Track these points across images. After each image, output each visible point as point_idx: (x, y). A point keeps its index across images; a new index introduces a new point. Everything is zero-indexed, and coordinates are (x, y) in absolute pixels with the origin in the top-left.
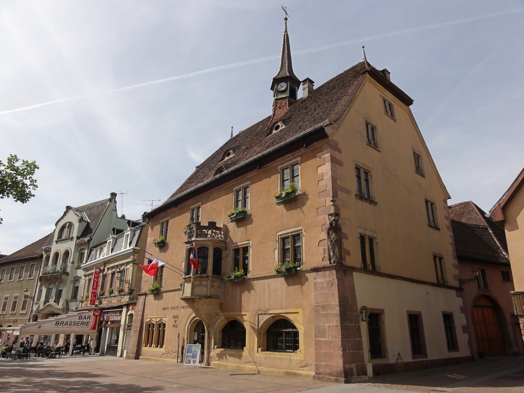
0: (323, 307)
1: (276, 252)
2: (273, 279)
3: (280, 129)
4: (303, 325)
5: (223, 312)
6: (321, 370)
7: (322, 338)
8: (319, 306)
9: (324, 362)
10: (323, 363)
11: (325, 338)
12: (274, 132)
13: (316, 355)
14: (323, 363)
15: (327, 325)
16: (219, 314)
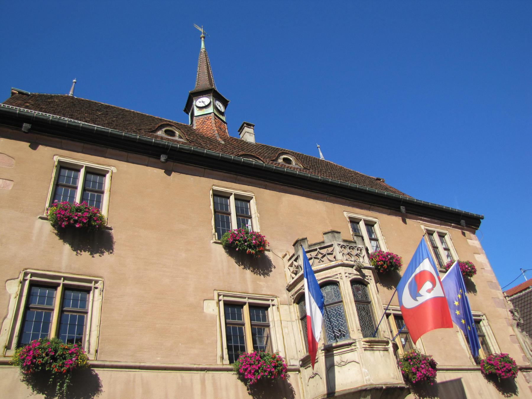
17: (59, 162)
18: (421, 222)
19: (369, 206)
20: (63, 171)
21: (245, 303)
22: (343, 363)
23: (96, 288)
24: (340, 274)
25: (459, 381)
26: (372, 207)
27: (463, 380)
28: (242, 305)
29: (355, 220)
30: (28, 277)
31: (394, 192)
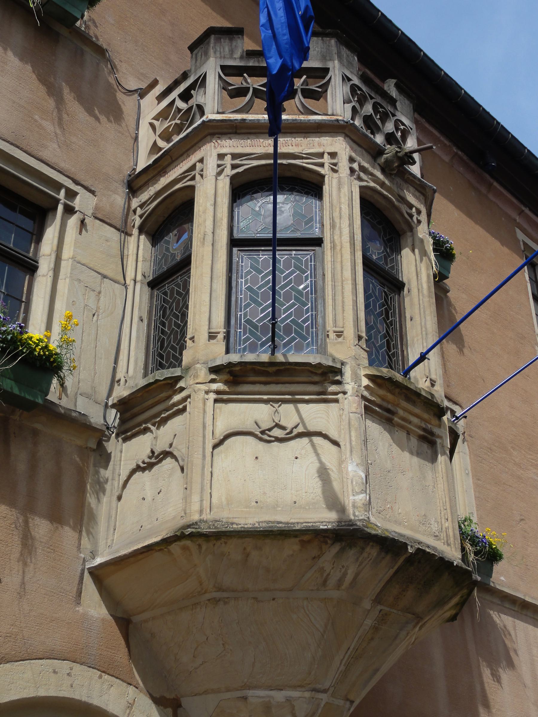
22: (277, 433)
24: (333, 155)
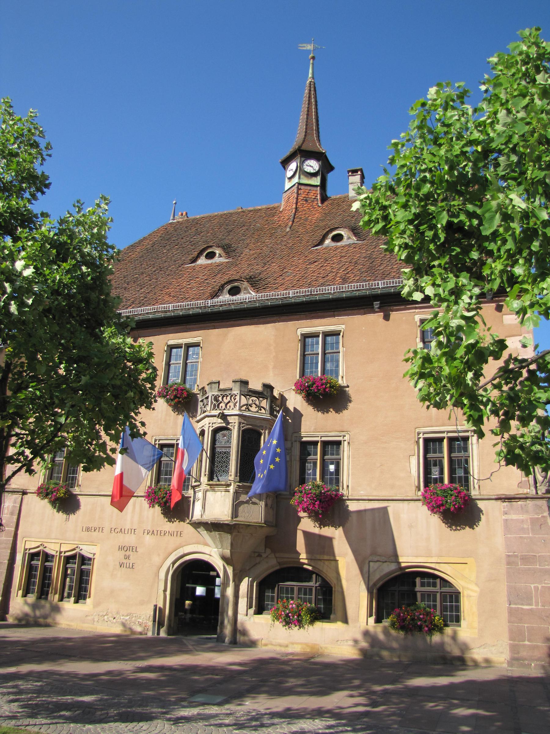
0: (525, 559)
1: (414, 461)
2: (8, 558)
3: (217, 260)
4: (476, 584)
5: (274, 551)
6: (524, 653)
7: (522, 604)
8: (516, 556)
9: (529, 641)
10: (527, 643)
11: (530, 604)
12: (202, 261)
13: (511, 631)
14: (527, 643)
15: (532, 586)
16: (264, 556)
17: (302, 335)
18: (417, 311)
19: (332, 313)
20: (307, 340)
21: (444, 438)
23: (345, 441)
25: (385, 509)
26: (336, 313)
27: (389, 509)
28: (441, 440)
29: (313, 335)
30: (421, 435)
31: (221, 306)
